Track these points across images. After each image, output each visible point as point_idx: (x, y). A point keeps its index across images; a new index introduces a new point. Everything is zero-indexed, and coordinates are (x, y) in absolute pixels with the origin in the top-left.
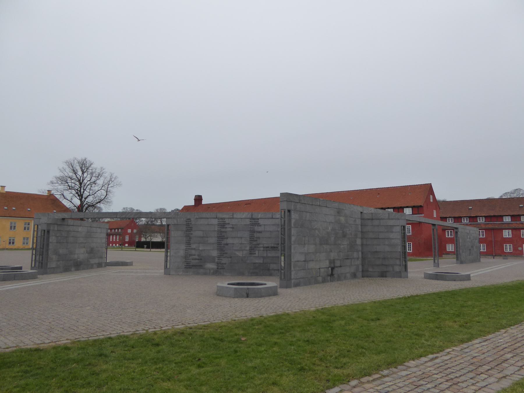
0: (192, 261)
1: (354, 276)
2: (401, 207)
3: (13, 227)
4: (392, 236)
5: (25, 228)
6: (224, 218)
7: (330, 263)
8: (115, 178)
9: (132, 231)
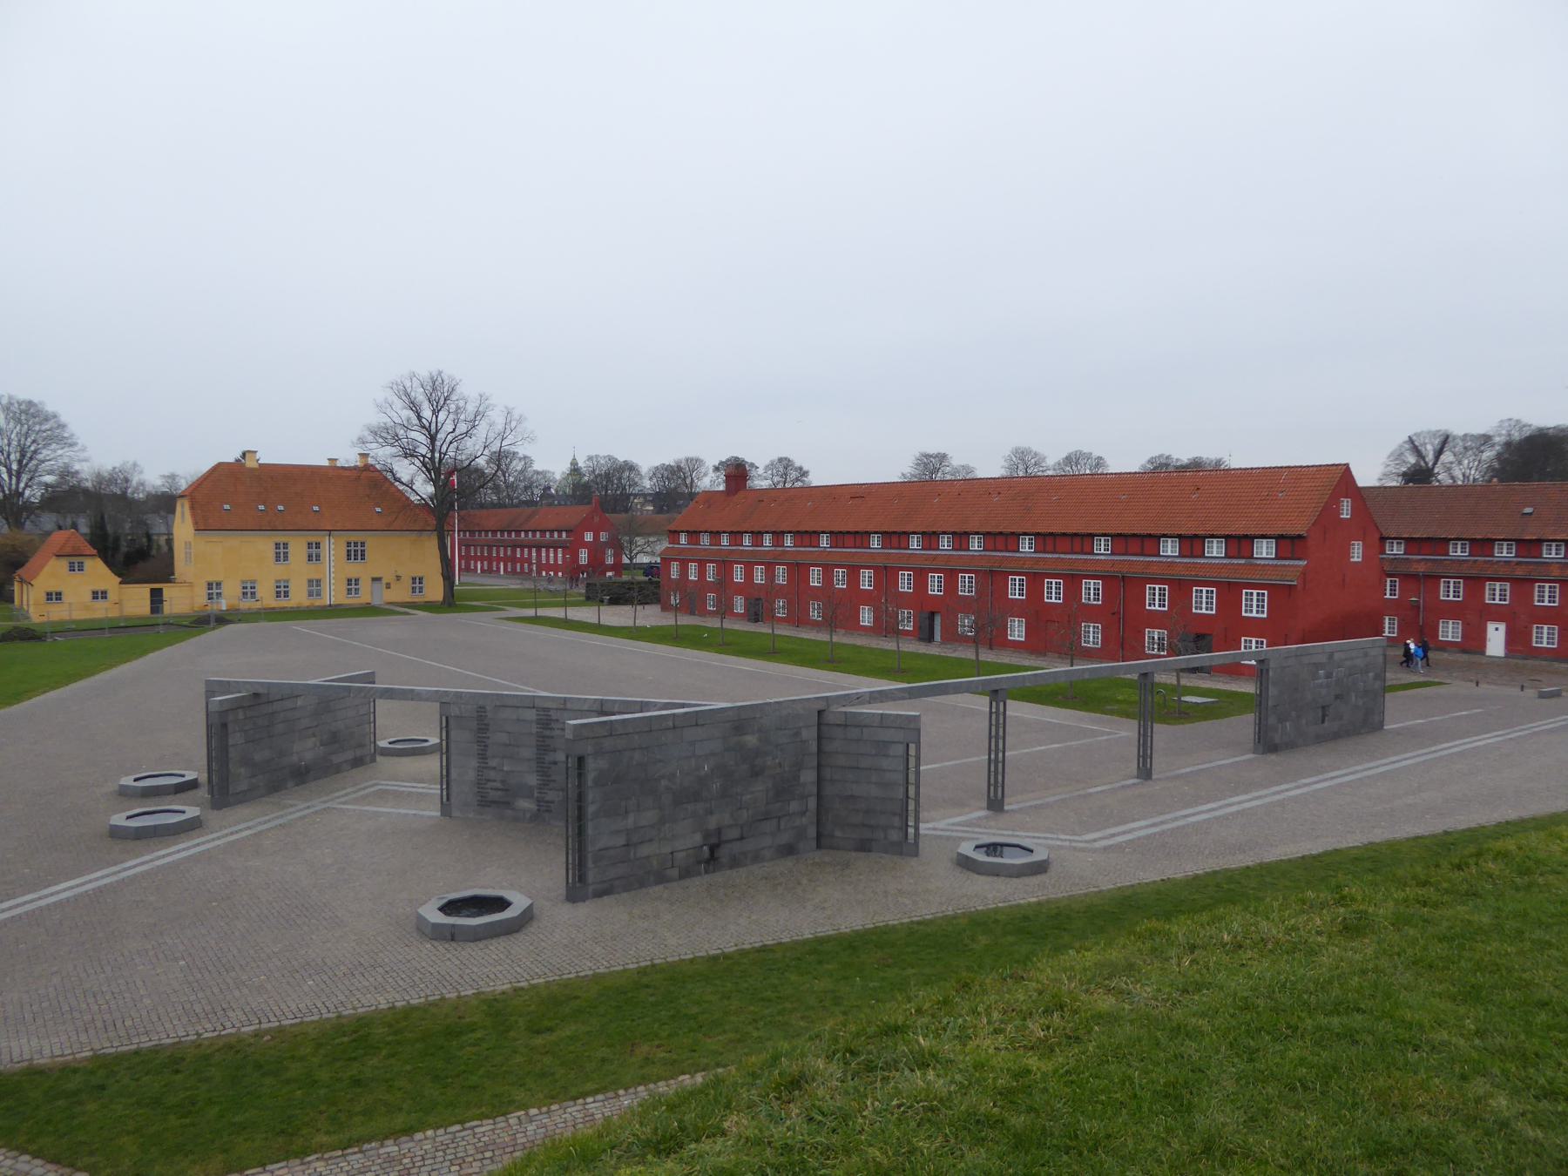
0: (492, 793)
1: (789, 850)
2: (1246, 536)
3: (281, 554)
4: (885, 763)
5: (310, 558)
6: (548, 709)
7: (707, 835)
8: (519, 421)
9: (596, 537)
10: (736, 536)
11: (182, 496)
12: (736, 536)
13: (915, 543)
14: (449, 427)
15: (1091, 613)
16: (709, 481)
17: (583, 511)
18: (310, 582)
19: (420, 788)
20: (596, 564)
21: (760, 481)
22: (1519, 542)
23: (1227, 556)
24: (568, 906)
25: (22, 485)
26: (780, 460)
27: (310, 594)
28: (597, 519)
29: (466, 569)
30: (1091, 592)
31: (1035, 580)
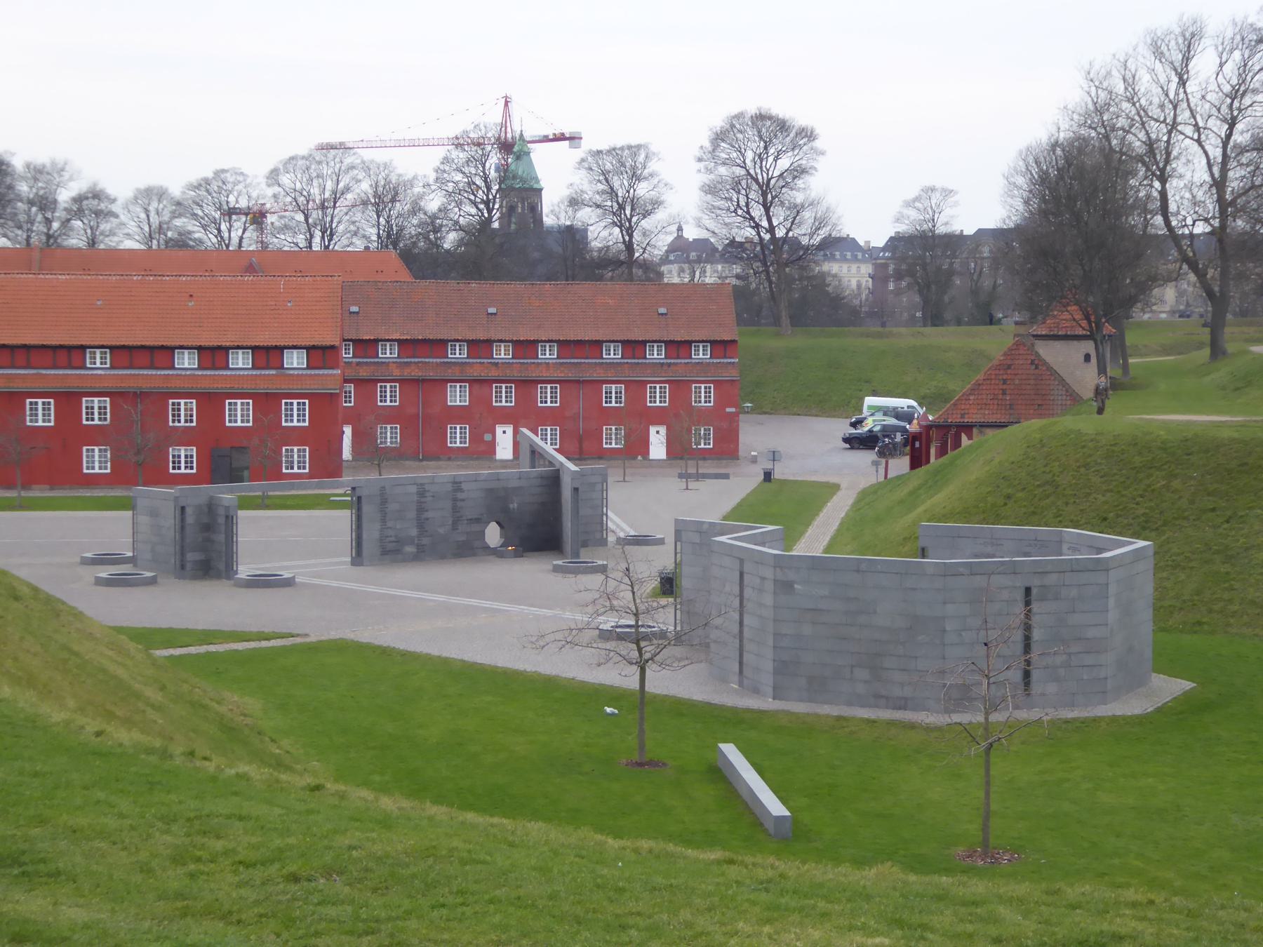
22: (713, 343)
23: (254, 367)
30: (96, 411)
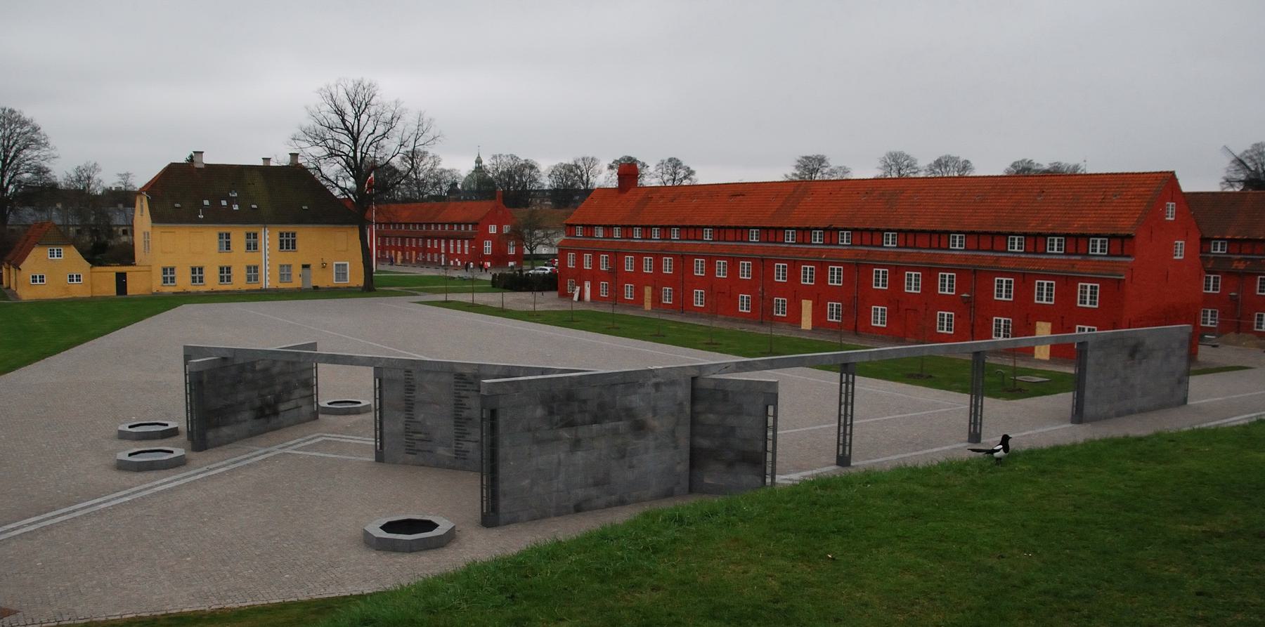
9: (499, 230)
10: (627, 229)
11: (140, 193)
12: (627, 229)
13: (790, 237)
14: (369, 129)
15: (946, 303)
16: (605, 178)
17: (485, 207)
18: (249, 268)
19: (357, 440)
20: (499, 258)
21: (650, 179)
24: (485, 530)
25: (6, 180)
26: (670, 160)
27: (249, 279)
28: (500, 212)
29: (381, 260)
31: (897, 273)
